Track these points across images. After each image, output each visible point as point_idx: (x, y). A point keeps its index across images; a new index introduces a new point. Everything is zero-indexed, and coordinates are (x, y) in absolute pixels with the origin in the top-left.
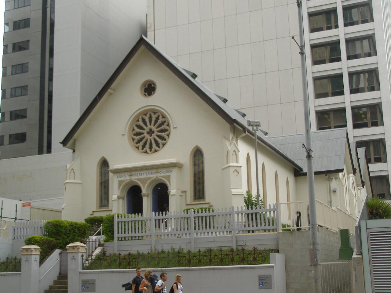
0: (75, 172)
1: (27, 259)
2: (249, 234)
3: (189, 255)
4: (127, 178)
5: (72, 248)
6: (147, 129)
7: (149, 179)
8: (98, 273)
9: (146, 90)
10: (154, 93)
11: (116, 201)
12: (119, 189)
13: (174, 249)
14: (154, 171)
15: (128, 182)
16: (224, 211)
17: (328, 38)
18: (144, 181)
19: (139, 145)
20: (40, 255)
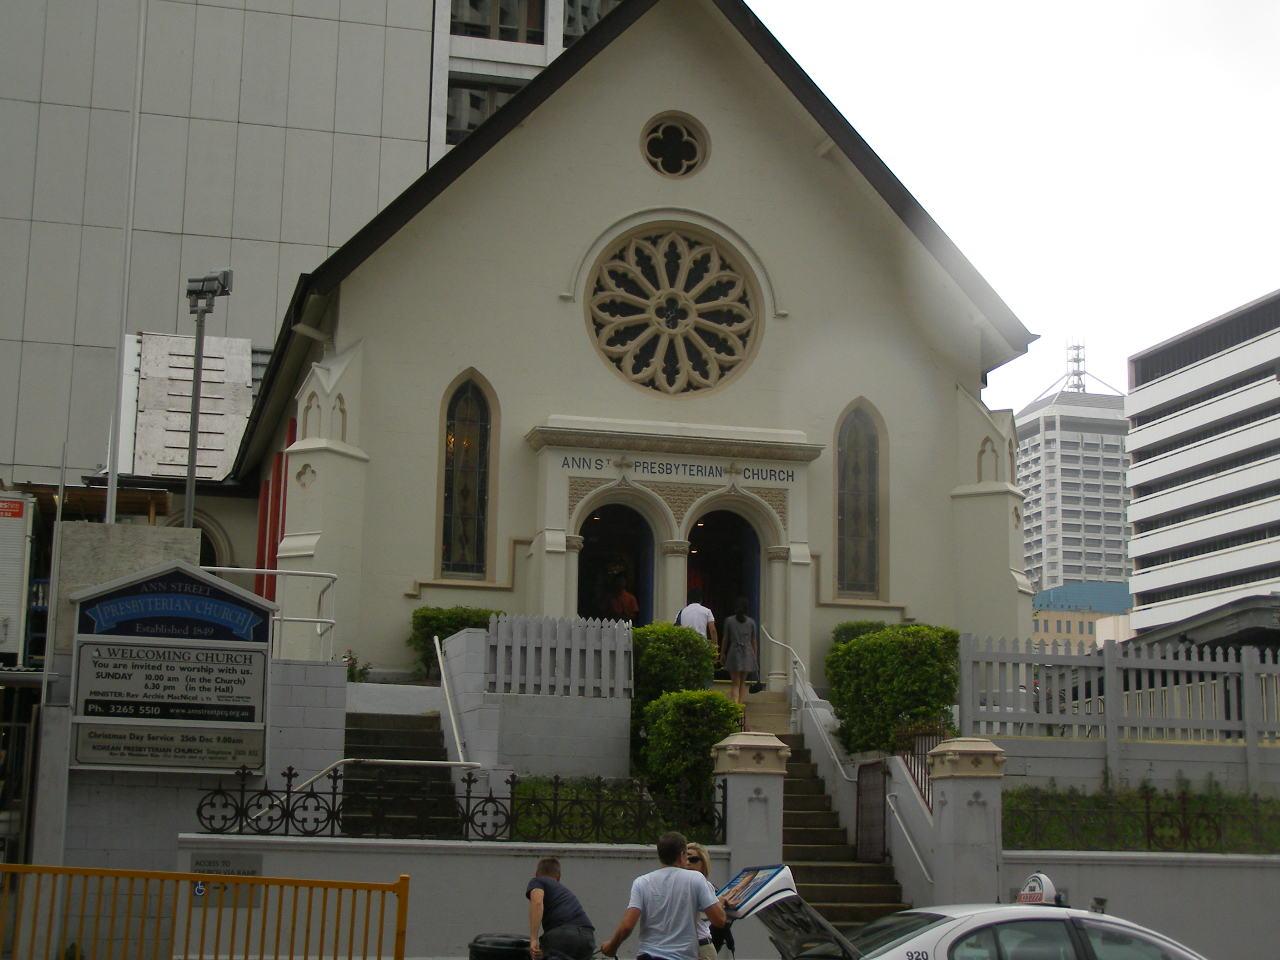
0: (996, 448)
1: (758, 791)
2: (1050, 738)
3: (1148, 808)
4: (607, 474)
5: (972, 758)
6: (658, 297)
7: (701, 489)
8: (1079, 865)
9: (672, 133)
10: (654, 165)
11: (564, 557)
12: (571, 509)
13: (1187, 783)
14: (725, 464)
15: (611, 489)
16: (996, 649)
17: (507, 67)
18: (680, 495)
19: (626, 353)
20: (785, 776)
